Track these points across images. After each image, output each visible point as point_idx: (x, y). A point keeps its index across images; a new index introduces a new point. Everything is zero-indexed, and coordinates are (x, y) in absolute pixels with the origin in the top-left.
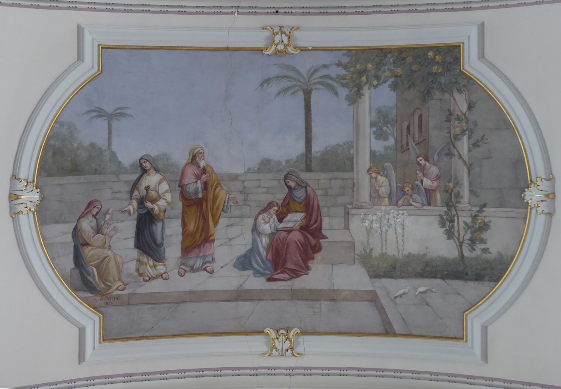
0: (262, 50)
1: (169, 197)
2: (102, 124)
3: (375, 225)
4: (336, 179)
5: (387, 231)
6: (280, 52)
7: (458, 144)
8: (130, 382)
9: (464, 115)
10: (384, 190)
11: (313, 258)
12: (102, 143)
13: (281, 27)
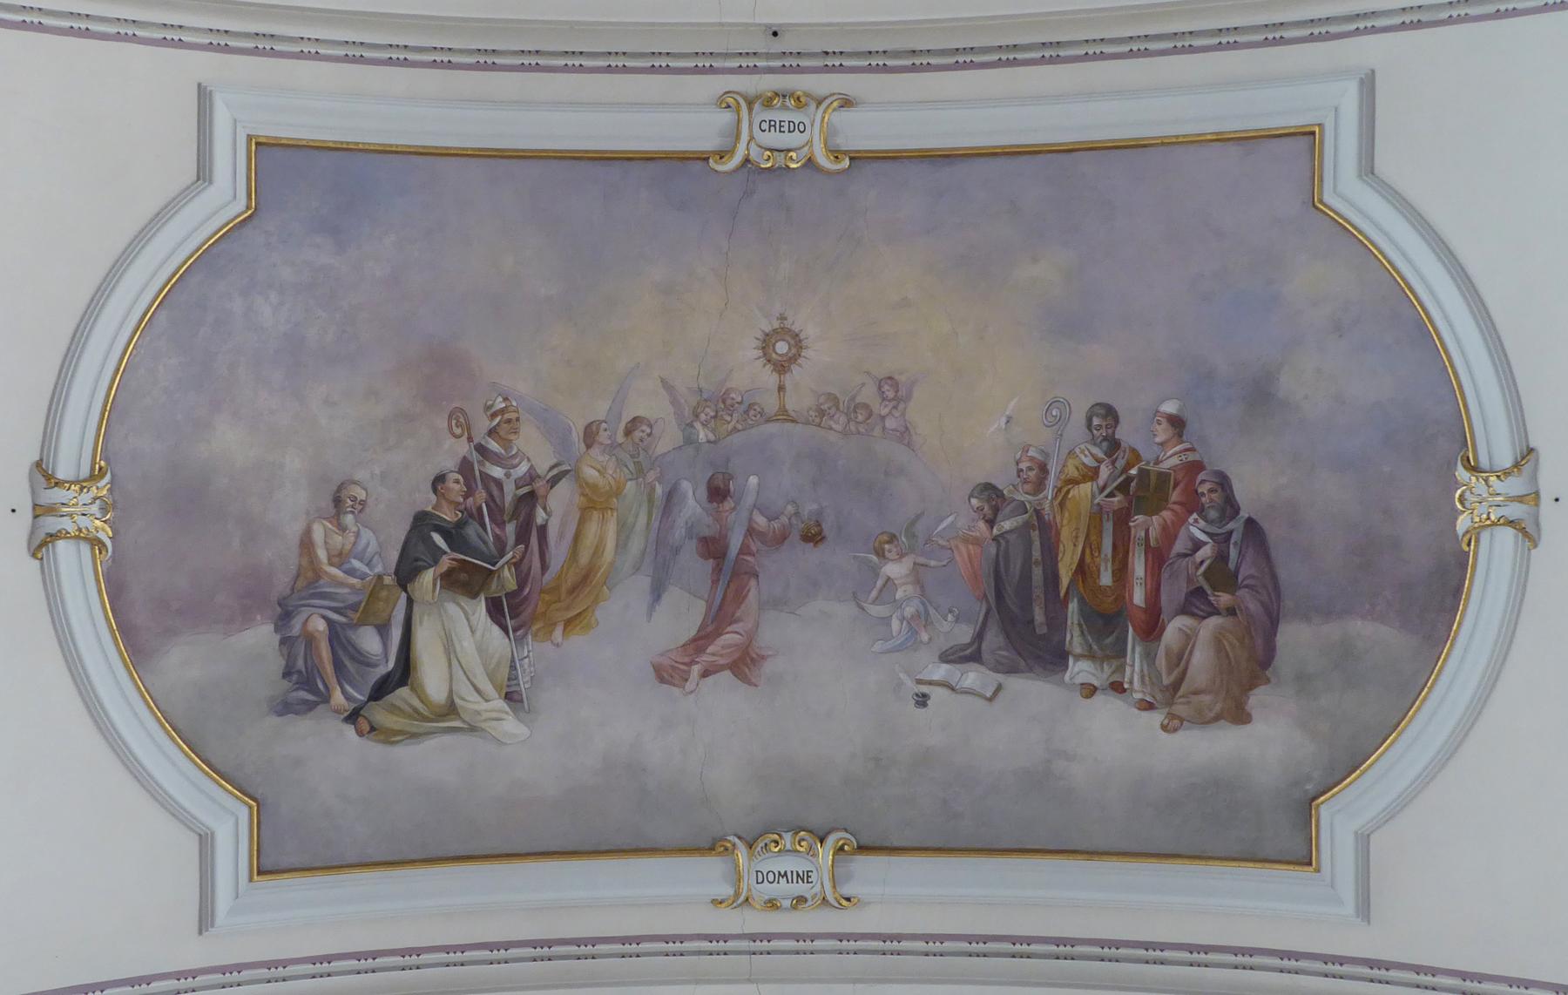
0: (707, 159)
8: (284, 980)
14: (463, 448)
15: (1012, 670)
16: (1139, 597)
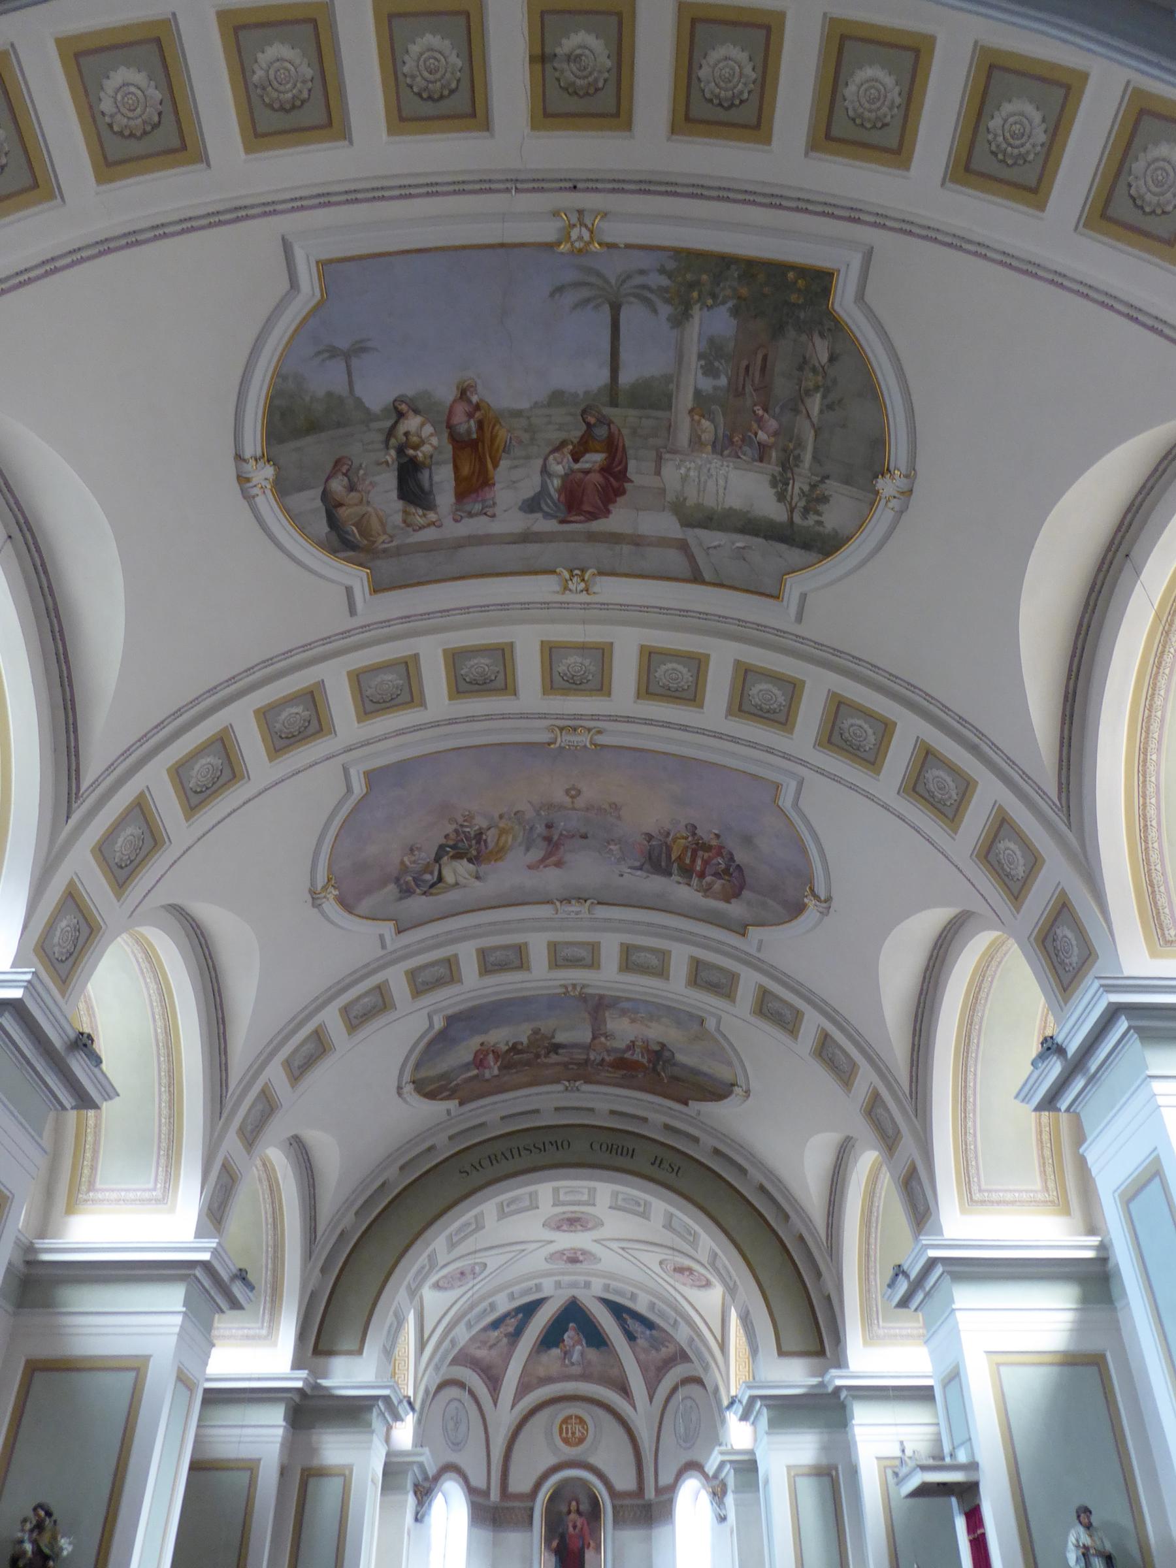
1: (434, 441)
2: (338, 366)
3: (692, 473)
4: (648, 417)
5: (706, 482)
6: (580, 250)
7: (808, 401)
9: (823, 367)
10: (707, 437)
11: (615, 502)
12: (341, 388)
13: (580, 212)
14: (454, 826)
15: (652, 873)
16: (698, 868)
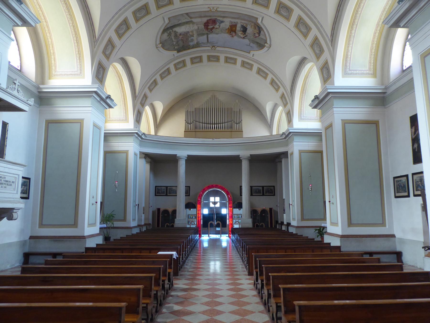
3: (192, 28)
